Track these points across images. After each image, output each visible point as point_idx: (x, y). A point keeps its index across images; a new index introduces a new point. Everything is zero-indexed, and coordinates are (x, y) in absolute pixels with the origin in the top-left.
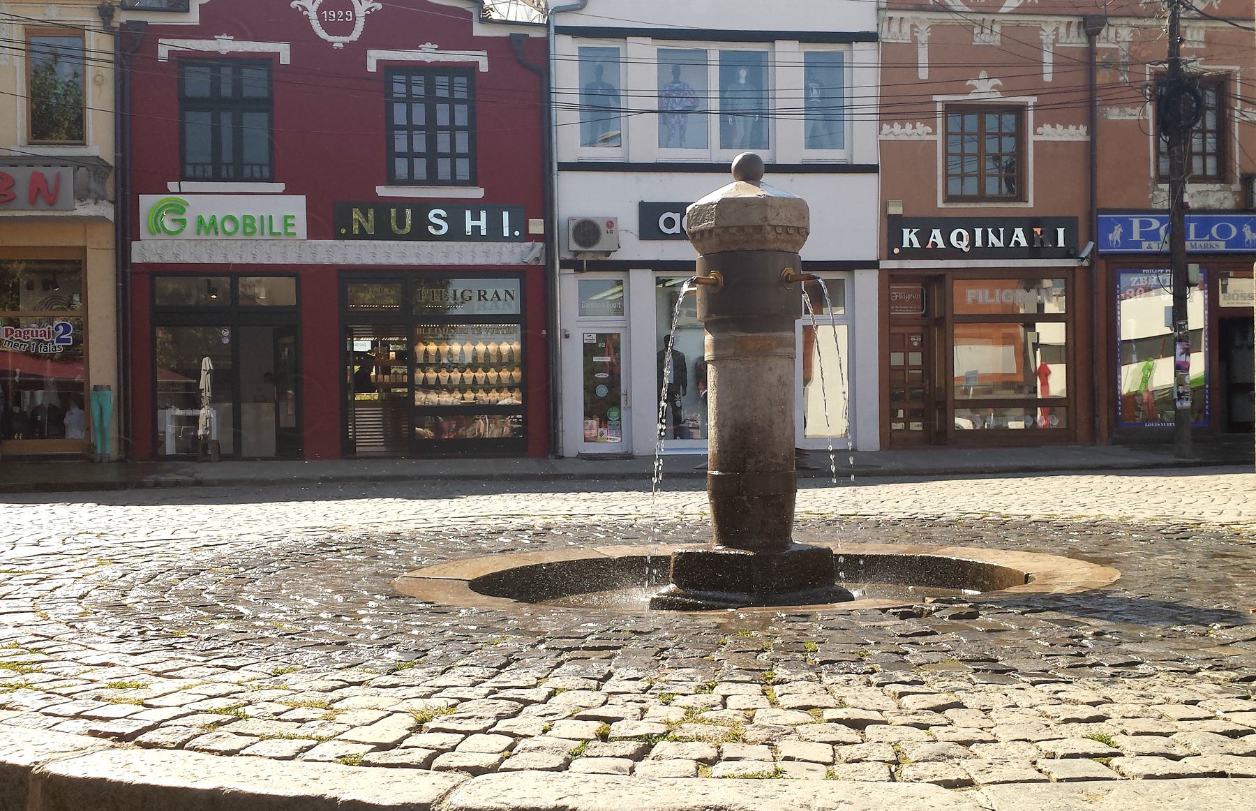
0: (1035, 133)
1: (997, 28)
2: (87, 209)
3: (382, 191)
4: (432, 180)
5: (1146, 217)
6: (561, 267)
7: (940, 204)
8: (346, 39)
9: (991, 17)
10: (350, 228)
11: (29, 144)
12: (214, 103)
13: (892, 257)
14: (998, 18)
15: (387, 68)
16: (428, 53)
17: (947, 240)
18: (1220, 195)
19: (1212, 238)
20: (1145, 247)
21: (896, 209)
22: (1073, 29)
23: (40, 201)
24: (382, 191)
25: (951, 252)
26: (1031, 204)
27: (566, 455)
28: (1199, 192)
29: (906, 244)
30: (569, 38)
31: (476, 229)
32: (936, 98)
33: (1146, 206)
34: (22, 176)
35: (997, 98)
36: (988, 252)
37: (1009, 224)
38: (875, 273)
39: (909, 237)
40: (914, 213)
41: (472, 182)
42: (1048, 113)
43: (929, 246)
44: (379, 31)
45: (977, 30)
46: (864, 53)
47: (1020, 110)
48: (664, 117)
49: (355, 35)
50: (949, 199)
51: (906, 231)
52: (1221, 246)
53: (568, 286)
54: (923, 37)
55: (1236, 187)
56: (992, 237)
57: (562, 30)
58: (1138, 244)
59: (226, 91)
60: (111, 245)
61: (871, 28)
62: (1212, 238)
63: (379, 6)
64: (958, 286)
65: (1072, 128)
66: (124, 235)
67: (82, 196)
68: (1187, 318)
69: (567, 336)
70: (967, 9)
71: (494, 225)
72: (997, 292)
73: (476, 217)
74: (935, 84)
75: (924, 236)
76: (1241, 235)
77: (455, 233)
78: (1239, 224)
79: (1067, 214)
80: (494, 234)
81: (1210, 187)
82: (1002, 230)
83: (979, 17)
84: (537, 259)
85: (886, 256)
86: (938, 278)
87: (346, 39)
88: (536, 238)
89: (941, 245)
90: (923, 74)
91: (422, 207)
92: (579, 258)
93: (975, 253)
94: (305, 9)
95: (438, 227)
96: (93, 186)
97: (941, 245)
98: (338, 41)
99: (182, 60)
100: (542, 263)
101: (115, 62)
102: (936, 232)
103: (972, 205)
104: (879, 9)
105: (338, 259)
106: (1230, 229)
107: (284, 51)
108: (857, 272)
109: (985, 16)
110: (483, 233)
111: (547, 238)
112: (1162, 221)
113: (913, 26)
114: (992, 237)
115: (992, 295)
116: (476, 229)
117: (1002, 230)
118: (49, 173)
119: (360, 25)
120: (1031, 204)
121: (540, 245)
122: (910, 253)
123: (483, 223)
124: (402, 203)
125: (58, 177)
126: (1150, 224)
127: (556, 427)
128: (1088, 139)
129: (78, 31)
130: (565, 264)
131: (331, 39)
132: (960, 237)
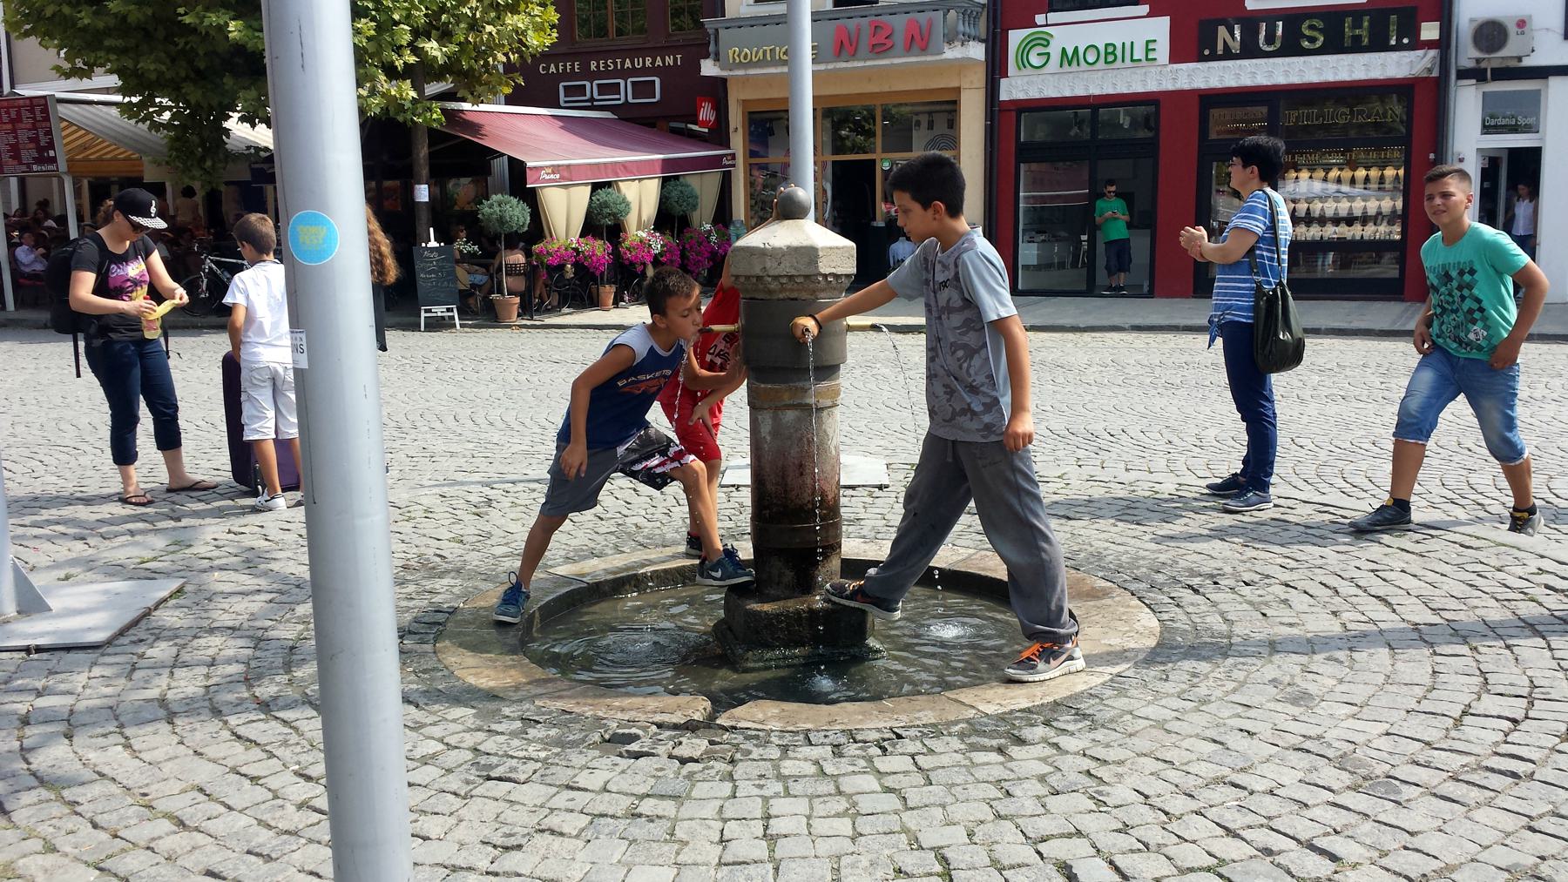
66: (993, 72)
84: (1430, 70)
88: (1430, 44)
92: (1483, 65)
100: (1435, 74)
105: (1200, 84)
111: (1443, 44)
116: (1357, 39)
121: (1433, 53)
130: (1463, 74)
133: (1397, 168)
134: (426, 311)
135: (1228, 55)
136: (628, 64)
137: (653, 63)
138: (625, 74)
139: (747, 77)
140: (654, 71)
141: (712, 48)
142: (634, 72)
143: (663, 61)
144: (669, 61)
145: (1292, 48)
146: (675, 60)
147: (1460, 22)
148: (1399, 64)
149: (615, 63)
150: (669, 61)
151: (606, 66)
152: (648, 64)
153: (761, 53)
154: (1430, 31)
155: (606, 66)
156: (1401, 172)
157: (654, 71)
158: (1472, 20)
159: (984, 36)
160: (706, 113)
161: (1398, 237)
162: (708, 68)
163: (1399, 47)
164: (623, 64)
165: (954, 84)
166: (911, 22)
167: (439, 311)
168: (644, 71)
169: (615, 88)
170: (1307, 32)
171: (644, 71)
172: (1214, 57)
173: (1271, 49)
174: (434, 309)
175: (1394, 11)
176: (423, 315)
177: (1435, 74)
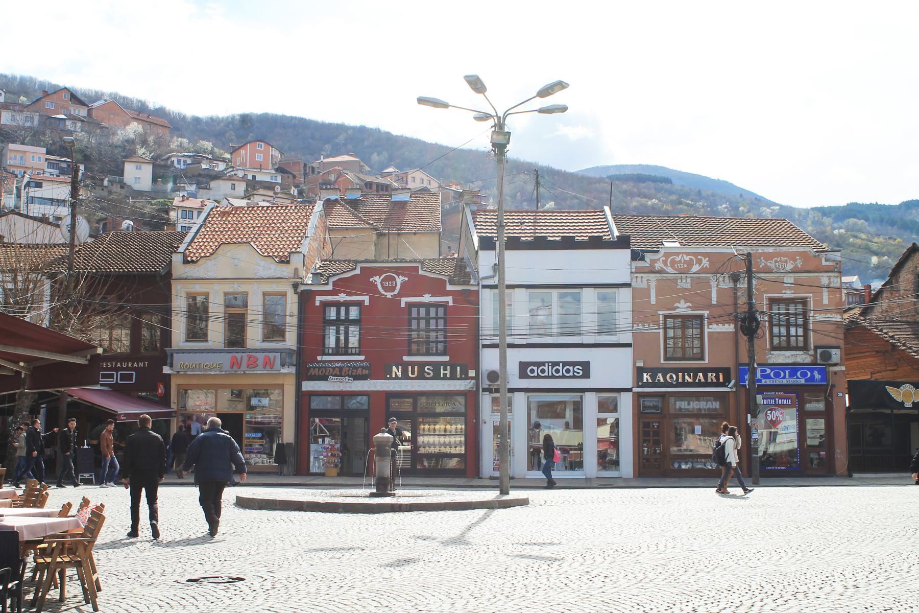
0: (708, 328)
1: (689, 280)
2: (285, 370)
3: (405, 358)
4: (428, 353)
5: (764, 368)
6: (483, 391)
7: (662, 361)
8: (392, 294)
9: (686, 275)
10: (391, 375)
11: (264, 341)
12: (337, 322)
13: (639, 386)
14: (688, 275)
15: (410, 305)
16: (427, 298)
17: (664, 378)
18: (804, 356)
19: (798, 378)
20: (763, 382)
21: (640, 364)
22: (727, 279)
23: (268, 367)
24: (405, 358)
25: (666, 384)
26: (707, 361)
27: (484, 476)
28: (792, 355)
29: (645, 380)
30: (489, 289)
31: (445, 375)
32: (659, 312)
33: (764, 362)
34: (260, 356)
35: (690, 312)
36: (685, 384)
37: (696, 371)
38: (631, 394)
39: (646, 377)
40: (649, 365)
41: (444, 354)
42: (713, 319)
43: (656, 381)
44: (406, 290)
45: (679, 281)
46: (625, 295)
47: (701, 317)
48: (603, 298)
49: (396, 292)
50: (666, 359)
51: (645, 375)
52: (803, 381)
53: (486, 400)
54: (653, 284)
55: (811, 352)
56: (687, 377)
57: (484, 287)
58: (760, 381)
59: (343, 309)
60: (294, 383)
61: (628, 281)
62: (798, 378)
63: (406, 279)
64: (672, 400)
65: (727, 325)
66: (299, 380)
67: (283, 365)
68: (846, 415)
69: (485, 423)
70: (674, 272)
71: (453, 372)
72: (691, 403)
73: (445, 369)
74: (660, 305)
75: (653, 377)
76: (813, 376)
77: (437, 377)
78: (812, 371)
79: (725, 366)
80: (453, 377)
81: (798, 352)
82: (692, 374)
83: (680, 275)
84: (472, 388)
85: (636, 386)
86: (663, 395)
87: (392, 294)
88: (472, 378)
89: (662, 381)
90: (653, 300)
91: (422, 365)
92: (491, 387)
93: (679, 385)
94: (376, 281)
95: (429, 374)
96: (288, 360)
97: (662, 381)
98: (389, 295)
99: (326, 305)
100: (474, 389)
101: (298, 327)
102: (660, 375)
103: (678, 362)
104: (631, 273)
105: (385, 388)
106: (801, 375)
107: (366, 299)
108: (622, 393)
109: (682, 275)
110: (448, 376)
111: (476, 378)
112: (772, 370)
113: (648, 280)
114: (687, 377)
115: (689, 404)
116: (445, 375)
117: (692, 374)
118: (271, 355)
119: (398, 287)
120: (707, 361)
121: (473, 381)
122: (647, 385)
123: (448, 372)
124: (413, 364)
125: (275, 357)
126: (766, 371)
127: (479, 464)
128: (734, 330)
129: (284, 294)
130: (484, 390)
131: (385, 294)
132: (671, 377)
133: (462, 425)
134: (81, 476)
135: (397, 378)
136: (119, 365)
137: (132, 365)
138: (117, 369)
139: (256, 374)
140: (132, 369)
141: (169, 361)
142: (122, 369)
143: (138, 364)
144: (141, 364)
145: (421, 376)
146: (144, 364)
147: (483, 368)
148: (460, 385)
149: (112, 364)
150: (141, 364)
151: (107, 365)
152: (130, 365)
153: (194, 365)
154: (472, 373)
155: (107, 365)
156: (463, 427)
157: (132, 369)
158: (486, 370)
159: (295, 363)
160: (161, 390)
161: (463, 452)
162: (166, 370)
163: (461, 379)
164: (116, 365)
165: (281, 382)
166: (266, 356)
167: (87, 476)
168: (127, 369)
169: (111, 376)
170: (427, 371)
171: (127, 369)
172: (391, 378)
173: (414, 376)
174: (85, 475)
175: (561, 362)
176: (80, 477)
177: (474, 389)
